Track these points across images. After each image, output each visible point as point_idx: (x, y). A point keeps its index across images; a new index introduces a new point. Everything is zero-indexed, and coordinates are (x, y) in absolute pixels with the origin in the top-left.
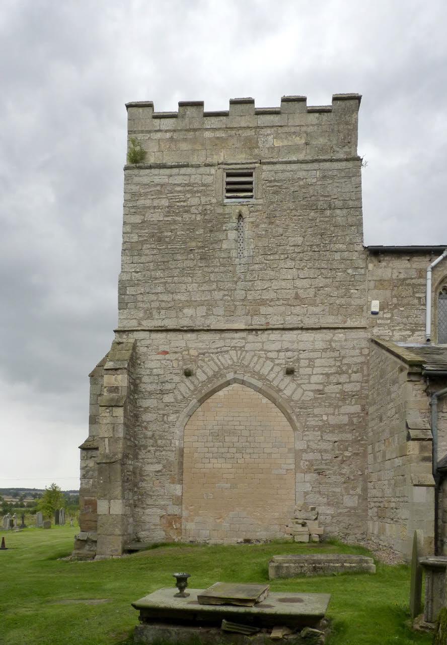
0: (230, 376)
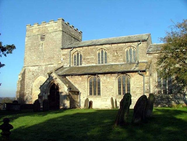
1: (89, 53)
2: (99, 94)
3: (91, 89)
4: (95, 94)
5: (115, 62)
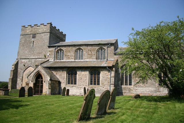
0: (29, 66)
1: (69, 51)
2: (75, 83)
3: (91, 79)
4: (72, 83)
5: (89, 59)
